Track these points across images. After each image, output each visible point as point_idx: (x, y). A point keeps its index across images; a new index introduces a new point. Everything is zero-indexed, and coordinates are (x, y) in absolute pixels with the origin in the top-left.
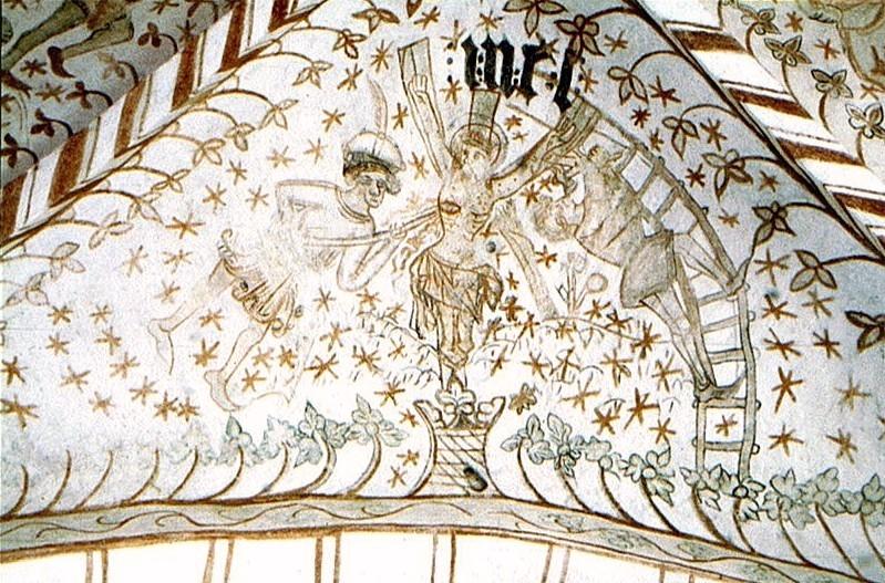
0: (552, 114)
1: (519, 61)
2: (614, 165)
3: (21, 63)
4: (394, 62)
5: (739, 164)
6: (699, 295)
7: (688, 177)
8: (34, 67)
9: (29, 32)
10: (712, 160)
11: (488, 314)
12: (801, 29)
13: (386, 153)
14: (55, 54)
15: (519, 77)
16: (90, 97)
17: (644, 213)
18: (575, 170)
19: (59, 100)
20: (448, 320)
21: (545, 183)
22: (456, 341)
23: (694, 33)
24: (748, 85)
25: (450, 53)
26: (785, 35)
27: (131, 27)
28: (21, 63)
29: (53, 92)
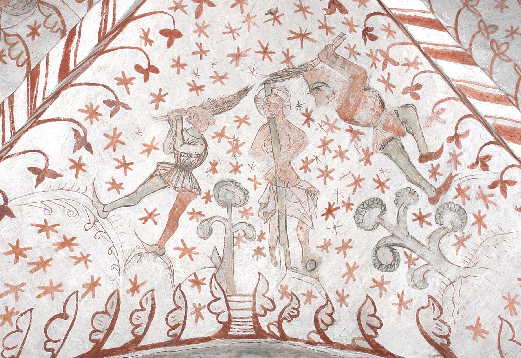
3: (431, 181)
8: (434, 172)
9: (407, 176)
14: (423, 159)
16: (460, 132)
19: (461, 154)
27: (406, 106)
28: (431, 181)
29: (455, 159)
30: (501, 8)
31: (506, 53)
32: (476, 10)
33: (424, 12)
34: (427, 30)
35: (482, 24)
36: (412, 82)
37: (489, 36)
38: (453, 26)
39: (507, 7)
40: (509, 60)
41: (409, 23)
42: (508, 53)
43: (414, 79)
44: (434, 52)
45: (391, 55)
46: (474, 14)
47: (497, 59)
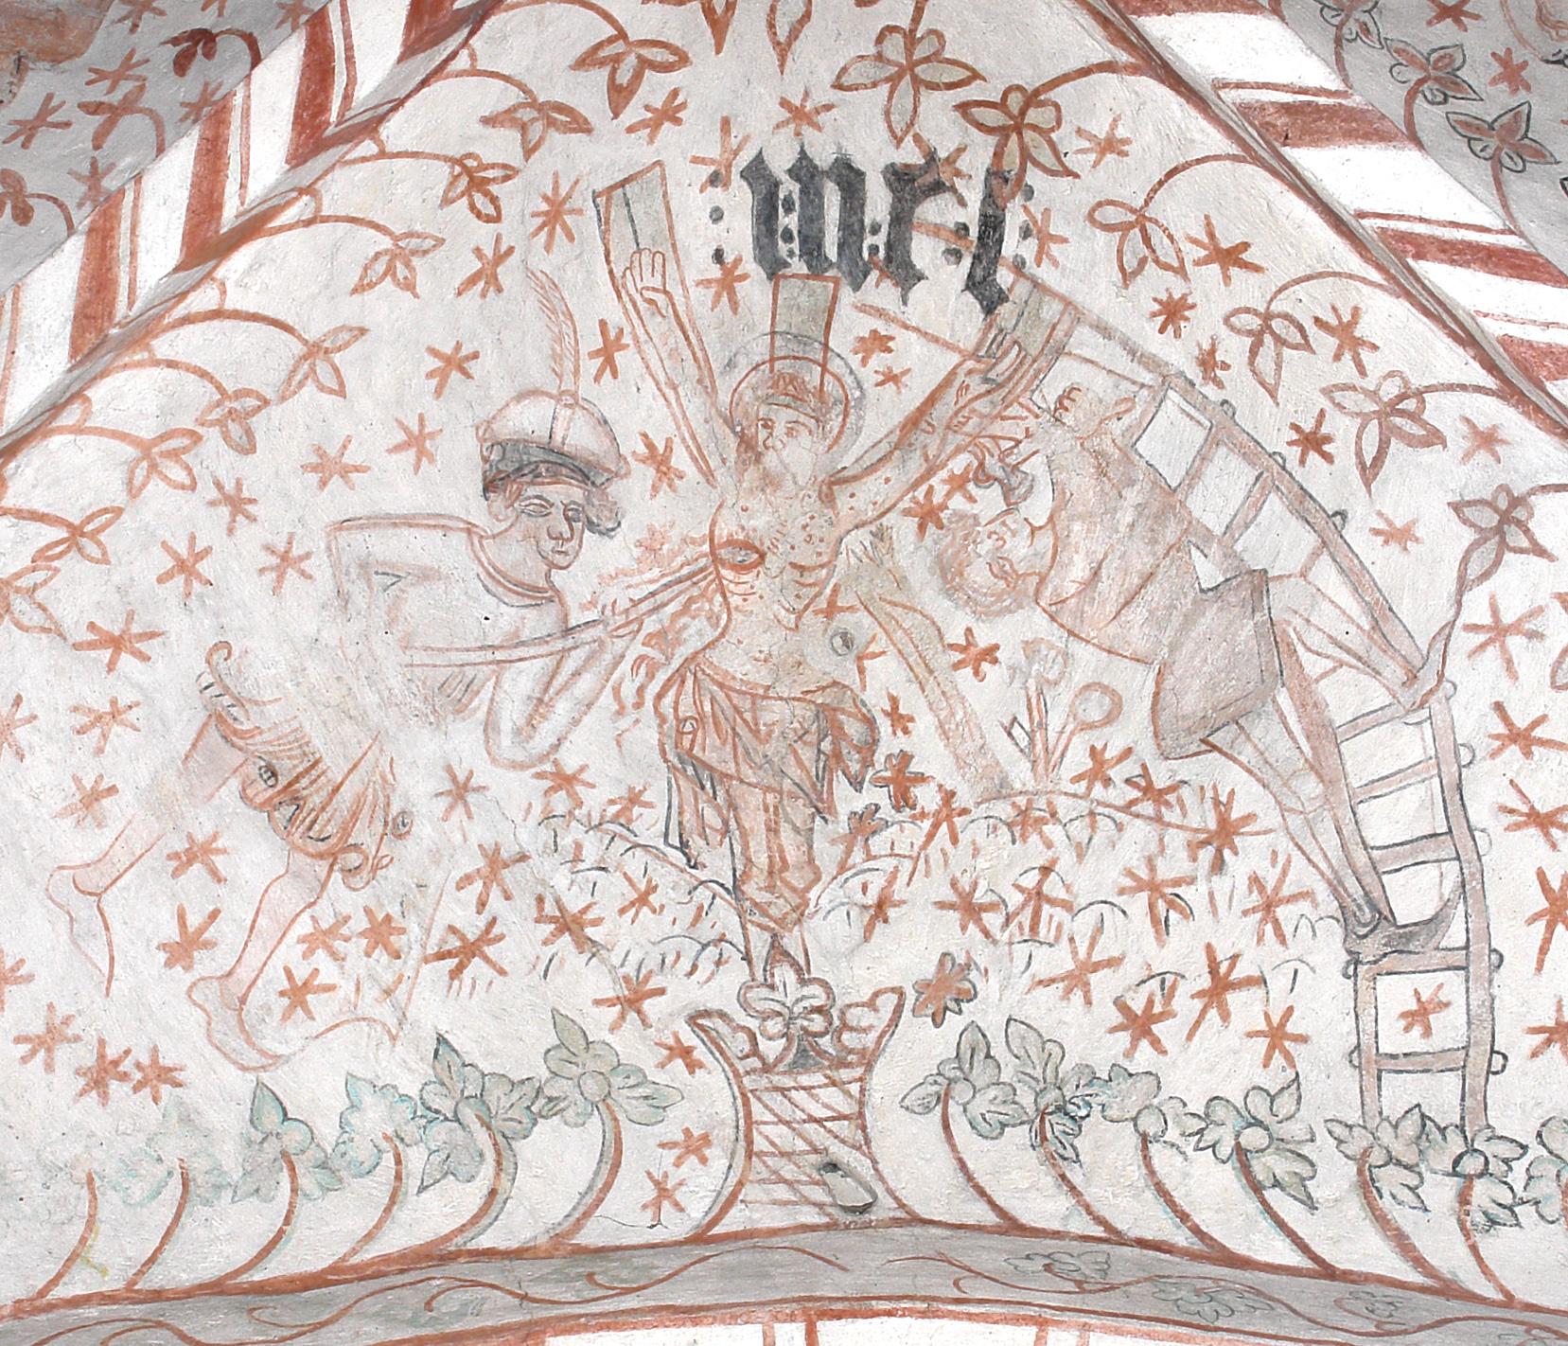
0: (965, 320)
1: (878, 203)
2: (1117, 427)
4: (587, 225)
5: (1410, 405)
6: (1340, 715)
7: (1291, 443)
10: (1349, 399)
11: (848, 800)
12: (1528, 88)
13: (579, 436)
15: (880, 240)
17: (1196, 536)
18: (1025, 447)
20: (754, 820)
21: (958, 483)
22: (777, 868)
23: (1286, 108)
24: (1421, 220)
25: (717, 194)
26: (1494, 102)
30: (318, 465)
31: (155, 480)
32: (301, 384)
33: (243, 186)
34: (182, 197)
35: (251, 402)
36: (39, 196)
37: (212, 424)
38: (229, 305)
39: (323, 483)
40: (133, 491)
41: (201, 138)
42: (156, 486)
43: (49, 198)
44: (108, 225)
45: (126, 122)
46: (284, 375)
47: (130, 452)
